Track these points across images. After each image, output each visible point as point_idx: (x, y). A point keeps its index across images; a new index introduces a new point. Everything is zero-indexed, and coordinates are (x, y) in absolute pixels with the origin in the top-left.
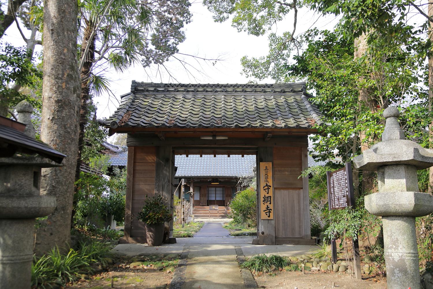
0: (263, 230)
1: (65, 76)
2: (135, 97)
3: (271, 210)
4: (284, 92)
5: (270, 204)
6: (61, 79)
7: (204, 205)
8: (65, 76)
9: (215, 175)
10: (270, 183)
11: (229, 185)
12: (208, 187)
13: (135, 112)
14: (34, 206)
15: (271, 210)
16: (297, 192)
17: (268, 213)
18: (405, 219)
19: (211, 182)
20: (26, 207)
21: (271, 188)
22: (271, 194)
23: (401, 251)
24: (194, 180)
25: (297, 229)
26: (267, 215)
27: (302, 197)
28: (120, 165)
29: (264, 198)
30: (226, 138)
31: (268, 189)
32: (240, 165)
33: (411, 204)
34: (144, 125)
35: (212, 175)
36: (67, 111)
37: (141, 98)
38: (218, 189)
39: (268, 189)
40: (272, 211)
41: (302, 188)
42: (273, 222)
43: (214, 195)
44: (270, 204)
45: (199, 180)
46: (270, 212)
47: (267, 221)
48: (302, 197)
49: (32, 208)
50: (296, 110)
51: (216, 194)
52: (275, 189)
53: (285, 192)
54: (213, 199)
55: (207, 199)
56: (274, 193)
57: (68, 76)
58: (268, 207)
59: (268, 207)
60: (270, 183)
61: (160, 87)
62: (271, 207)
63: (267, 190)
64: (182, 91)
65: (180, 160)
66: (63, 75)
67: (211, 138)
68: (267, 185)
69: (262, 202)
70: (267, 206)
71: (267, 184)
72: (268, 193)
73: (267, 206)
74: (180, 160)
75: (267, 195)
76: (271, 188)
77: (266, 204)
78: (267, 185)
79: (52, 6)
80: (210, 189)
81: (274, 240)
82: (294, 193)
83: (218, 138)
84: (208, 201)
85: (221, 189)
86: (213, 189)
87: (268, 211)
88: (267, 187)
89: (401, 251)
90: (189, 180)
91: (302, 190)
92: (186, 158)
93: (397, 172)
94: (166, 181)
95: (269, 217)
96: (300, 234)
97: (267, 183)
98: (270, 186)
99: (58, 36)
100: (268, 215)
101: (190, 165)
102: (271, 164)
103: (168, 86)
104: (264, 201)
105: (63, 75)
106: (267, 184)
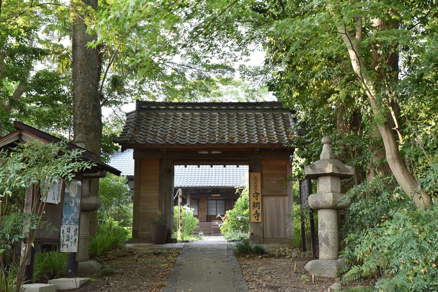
0: (252, 232)
1: (91, 106)
4: (272, 110)
5: (259, 209)
6: (89, 109)
7: (203, 220)
8: (91, 106)
9: (216, 185)
10: (259, 191)
12: (208, 200)
13: (142, 131)
14: (92, 202)
17: (257, 217)
19: (211, 194)
20: (87, 204)
22: (259, 200)
23: (326, 231)
24: (191, 192)
25: (282, 230)
27: (287, 203)
28: (129, 175)
30: (220, 152)
31: (257, 196)
32: (236, 176)
33: (331, 201)
34: (151, 143)
35: (212, 185)
36: (93, 134)
37: (145, 117)
38: (218, 202)
40: (260, 215)
41: (287, 195)
43: (215, 210)
44: (259, 209)
45: (197, 192)
46: (258, 216)
47: (256, 224)
48: (287, 203)
49: (91, 204)
50: (281, 128)
51: (216, 211)
52: (263, 196)
53: (272, 199)
55: (206, 214)
57: (93, 106)
58: (257, 212)
59: (257, 212)
61: (162, 106)
62: (260, 211)
63: (256, 197)
65: (178, 169)
66: (90, 106)
67: (207, 153)
68: (256, 193)
72: (257, 200)
74: (178, 169)
75: (256, 201)
76: (260, 195)
77: (255, 209)
78: (256, 193)
79: (80, 51)
80: (210, 202)
81: (262, 240)
82: (281, 199)
83: (213, 152)
84: (207, 216)
86: (214, 202)
88: (256, 195)
89: (326, 231)
90: (186, 190)
91: (287, 197)
92: (184, 168)
93: (326, 180)
95: (258, 220)
96: (285, 234)
98: (259, 194)
99: (85, 75)
101: (186, 176)
102: (259, 174)
104: (253, 207)
105: (90, 106)
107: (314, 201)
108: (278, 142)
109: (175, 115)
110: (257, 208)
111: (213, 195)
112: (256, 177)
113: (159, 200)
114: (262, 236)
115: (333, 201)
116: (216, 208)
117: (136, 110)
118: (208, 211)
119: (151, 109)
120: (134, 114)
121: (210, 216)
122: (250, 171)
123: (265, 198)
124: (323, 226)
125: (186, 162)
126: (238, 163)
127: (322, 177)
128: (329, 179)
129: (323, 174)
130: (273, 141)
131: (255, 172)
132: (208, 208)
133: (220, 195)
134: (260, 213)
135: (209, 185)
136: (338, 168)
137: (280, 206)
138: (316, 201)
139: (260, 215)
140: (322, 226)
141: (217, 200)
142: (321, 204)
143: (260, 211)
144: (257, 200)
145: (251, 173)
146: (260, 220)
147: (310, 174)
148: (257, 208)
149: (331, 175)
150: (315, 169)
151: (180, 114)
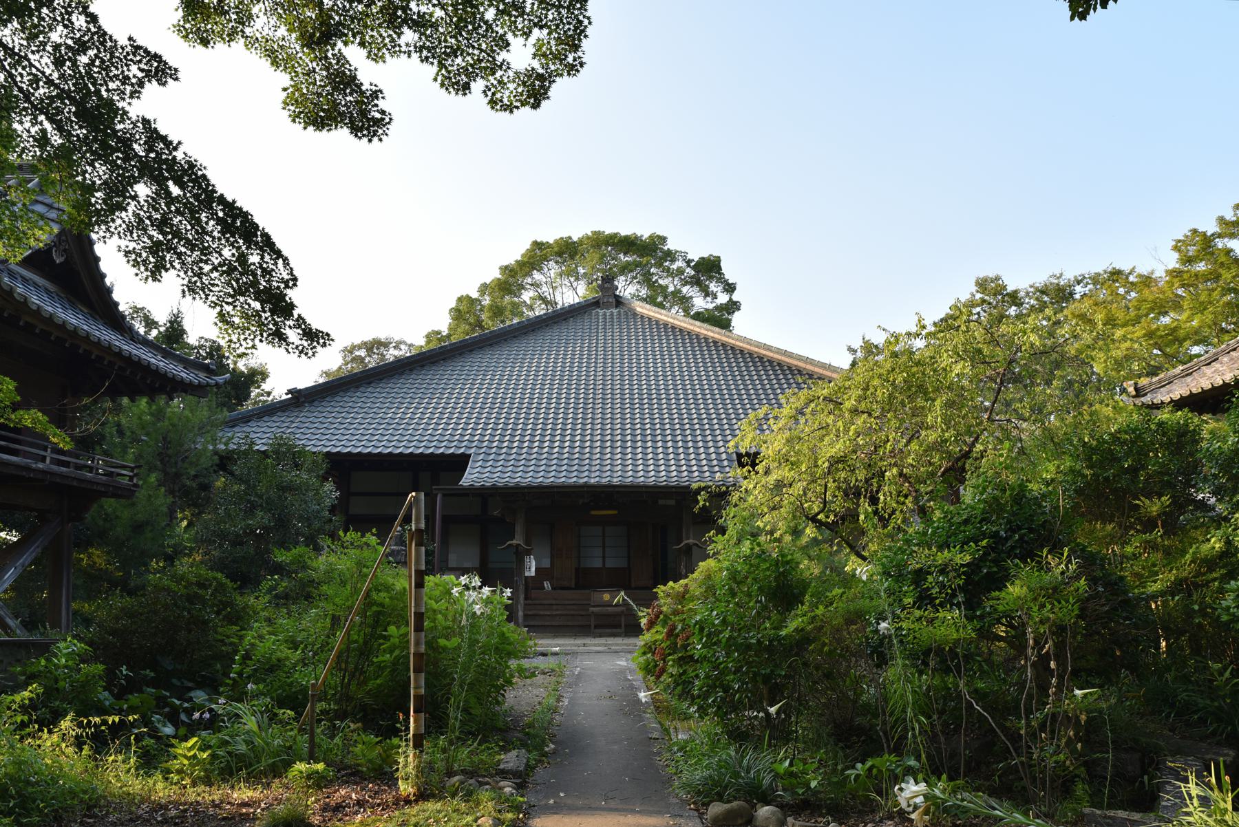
54: (597, 563)
84: (577, 570)
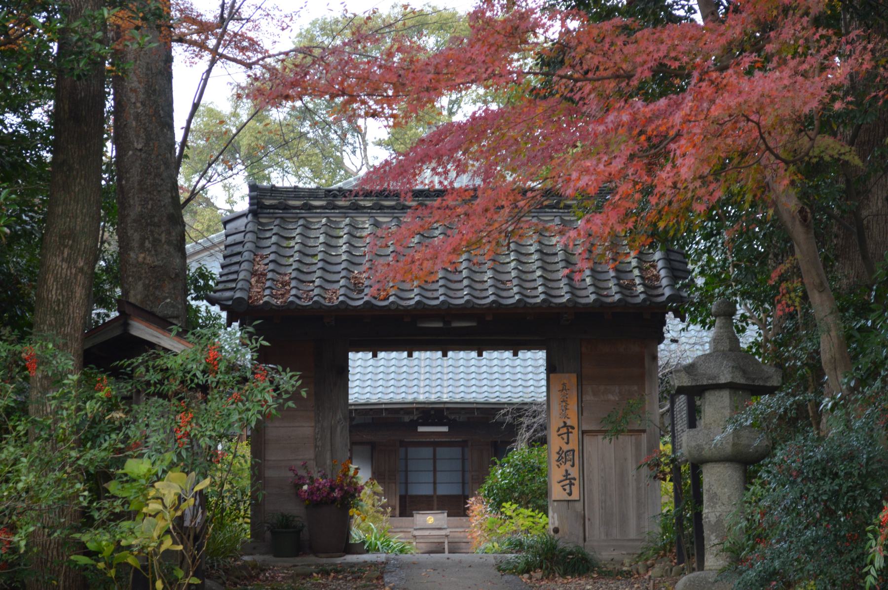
0: (556, 525)
2: (260, 224)
3: (575, 479)
5: (573, 466)
9: (433, 398)
10: (572, 421)
11: (482, 429)
15: (575, 479)
16: (634, 441)
17: (567, 487)
18: (727, 465)
21: (575, 431)
22: (574, 445)
23: (719, 509)
26: (565, 490)
29: (558, 453)
30: (474, 324)
31: (568, 433)
32: (513, 376)
38: (442, 452)
39: (568, 433)
40: (576, 482)
42: (579, 506)
44: (573, 466)
46: (571, 484)
47: (566, 503)
51: (435, 483)
54: (425, 490)
56: (582, 443)
60: (572, 421)
62: (574, 472)
63: (565, 436)
64: (369, 208)
65: (359, 363)
67: (439, 325)
68: (565, 425)
69: (554, 464)
70: (567, 471)
71: (565, 423)
72: (567, 443)
73: (567, 471)
74: (359, 363)
75: (566, 448)
76: (575, 431)
77: (563, 468)
78: (565, 425)
83: (456, 324)
85: (456, 452)
86: (427, 452)
87: (568, 482)
89: (719, 509)
94: (338, 418)
95: (570, 494)
97: (566, 420)
98: (573, 428)
100: (568, 491)
101: (377, 378)
103: (335, 196)
104: (558, 461)
106: (565, 423)
107: (694, 444)
108: (619, 300)
109: (353, 226)
110: (569, 463)
111: (421, 429)
112: (564, 384)
113: (316, 446)
114: (581, 535)
115: (734, 445)
116: (435, 471)
117: (250, 211)
118: (406, 483)
119: (287, 208)
120: (244, 221)
121: (412, 497)
122: (551, 369)
123: (587, 439)
124: (714, 497)
125: (376, 343)
126: (515, 346)
127: (712, 392)
128: (725, 395)
129: (712, 385)
130: (607, 296)
131: (563, 372)
132: (406, 471)
133: (445, 429)
134: (577, 477)
135: (410, 398)
136: (744, 372)
137: (626, 459)
138: (698, 445)
139: (576, 482)
140: (711, 499)
141: (435, 445)
142: (706, 453)
143: (574, 472)
144: (567, 443)
145: (551, 375)
146: (575, 496)
147: (685, 384)
148: (570, 463)
149: (731, 386)
150: (696, 375)
151: (366, 223)
